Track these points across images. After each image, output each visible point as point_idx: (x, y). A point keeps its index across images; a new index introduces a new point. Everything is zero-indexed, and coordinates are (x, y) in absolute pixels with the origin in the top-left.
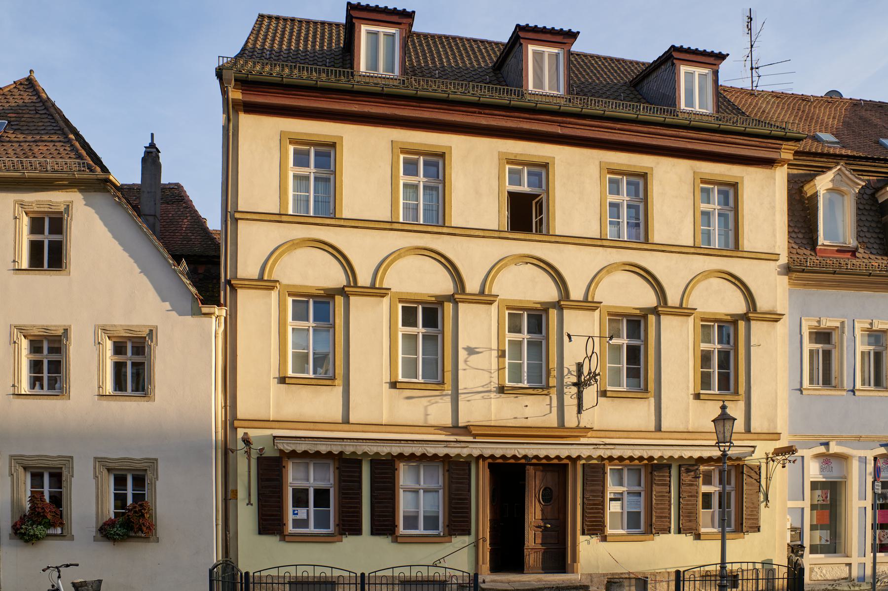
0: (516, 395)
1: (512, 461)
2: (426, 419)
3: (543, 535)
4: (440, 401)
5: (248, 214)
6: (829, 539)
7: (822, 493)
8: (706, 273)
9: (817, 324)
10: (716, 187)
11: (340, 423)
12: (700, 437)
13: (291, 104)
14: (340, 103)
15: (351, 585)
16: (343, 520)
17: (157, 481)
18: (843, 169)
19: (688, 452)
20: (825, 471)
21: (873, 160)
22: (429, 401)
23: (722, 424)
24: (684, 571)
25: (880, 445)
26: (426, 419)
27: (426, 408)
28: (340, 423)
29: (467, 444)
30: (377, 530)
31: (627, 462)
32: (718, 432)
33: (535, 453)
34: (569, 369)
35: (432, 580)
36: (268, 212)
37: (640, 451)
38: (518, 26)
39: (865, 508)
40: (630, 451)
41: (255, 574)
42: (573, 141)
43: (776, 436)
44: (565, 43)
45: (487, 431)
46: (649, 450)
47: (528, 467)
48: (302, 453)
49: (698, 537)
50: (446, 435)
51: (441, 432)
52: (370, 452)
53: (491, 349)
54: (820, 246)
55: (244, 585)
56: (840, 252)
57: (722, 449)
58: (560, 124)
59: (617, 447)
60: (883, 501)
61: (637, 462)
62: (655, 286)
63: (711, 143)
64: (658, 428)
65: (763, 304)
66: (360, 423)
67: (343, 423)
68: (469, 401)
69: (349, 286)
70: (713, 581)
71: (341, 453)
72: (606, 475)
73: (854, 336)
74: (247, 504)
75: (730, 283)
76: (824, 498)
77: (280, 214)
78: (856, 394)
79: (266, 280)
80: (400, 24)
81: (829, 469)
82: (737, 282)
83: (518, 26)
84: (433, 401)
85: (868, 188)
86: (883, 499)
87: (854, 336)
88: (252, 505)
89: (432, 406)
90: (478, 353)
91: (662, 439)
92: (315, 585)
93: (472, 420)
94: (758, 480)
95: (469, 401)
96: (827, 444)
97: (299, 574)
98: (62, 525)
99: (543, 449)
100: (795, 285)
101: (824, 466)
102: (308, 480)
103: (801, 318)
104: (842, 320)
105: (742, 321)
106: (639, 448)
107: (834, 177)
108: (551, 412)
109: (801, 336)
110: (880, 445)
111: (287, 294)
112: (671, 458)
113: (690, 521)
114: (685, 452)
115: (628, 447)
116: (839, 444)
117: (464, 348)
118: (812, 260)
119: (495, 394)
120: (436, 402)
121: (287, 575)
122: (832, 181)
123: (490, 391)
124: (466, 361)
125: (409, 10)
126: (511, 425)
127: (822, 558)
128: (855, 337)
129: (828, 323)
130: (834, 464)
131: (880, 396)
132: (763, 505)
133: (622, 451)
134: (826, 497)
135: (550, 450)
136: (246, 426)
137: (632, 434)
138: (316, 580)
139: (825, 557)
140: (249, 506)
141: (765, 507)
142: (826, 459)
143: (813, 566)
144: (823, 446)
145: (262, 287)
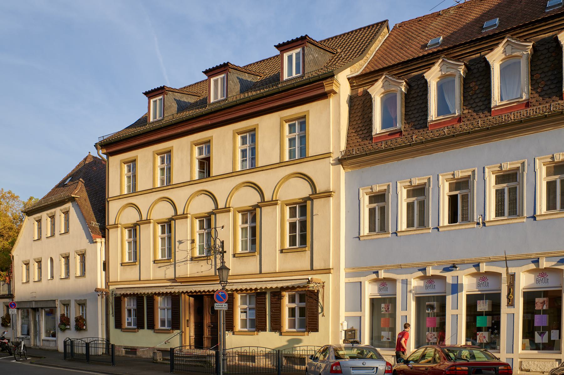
0: (198, 261)
1: (199, 294)
2: (165, 278)
3: (211, 330)
4: (170, 267)
6: (390, 338)
7: (385, 306)
8: (194, 194)
9: (370, 191)
10: (297, 121)
11: (258, 274)
12: (281, 275)
13: (288, 101)
18: (387, 76)
19: (270, 284)
20: (481, 286)
21: (525, 25)
22: (166, 268)
23: (227, 272)
25: (418, 270)
26: (165, 278)
27: (165, 271)
28: (258, 274)
29: (174, 287)
31: (245, 291)
32: (220, 275)
33: (199, 290)
34: (218, 245)
36: (216, 175)
37: (246, 285)
39: (406, 316)
40: (241, 286)
42: (218, 125)
43: (327, 271)
44: (226, 70)
45: (187, 279)
46: (250, 284)
47: (156, 297)
48: (270, 288)
49: (281, 334)
50: (171, 283)
51: (169, 282)
53: (187, 240)
54: (375, 135)
56: (391, 135)
57: (223, 285)
58: (209, 119)
59: (235, 284)
60: (431, 311)
61: (254, 291)
62: (259, 191)
63: (218, 117)
64: (261, 273)
65: (320, 188)
67: (311, 270)
68: (179, 266)
69: (313, 194)
72: (234, 299)
73: (484, 179)
75: (302, 179)
76: (386, 309)
77: (280, 163)
78: (486, 225)
79: (274, 200)
80: (163, 93)
81: (432, 287)
82: (305, 178)
84: (168, 268)
85: (414, 81)
86: (431, 309)
87: (484, 179)
89: (168, 269)
90: (183, 242)
91: (261, 278)
93: (180, 275)
94: (317, 299)
95: (179, 266)
96: (377, 273)
97: (243, 351)
98: (69, 325)
99: (203, 287)
100: (353, 168)
101: (428, 285)
102: (131, 305)
103: (359, 189)
104: (388, 184)
105: (309, 201)
106: (283, 282)
107: (383, 84)
108: (212, 268)
109: (359, 201)
110: (418, 270)
111: (491, 173)
113: (276, 324)
114: (268, 285)
115: (240, 284)
116: (387, 271)
117: (178, 241)
118: (368, 146)
119: (190, 261)
120: (169, 268)
121: (254, 351)
122: (383, 87)
123: (187, 260)
124: (178, 247)
125: (304, 35)
126: (196, 276)
127: (536, 354)
128: (485, 180)
130: (389, 285)
131: (416, 234)
132: (320, 316)
133: (237, 286)
134: (388, 309)
135: (205, 288)
136: (232, 278)
137: (246, 277)
139: (381, 350)
141: (322, 316)
142: (483, 277)
143: (523, 360)
144: (375, 274)
145: (324, 196)
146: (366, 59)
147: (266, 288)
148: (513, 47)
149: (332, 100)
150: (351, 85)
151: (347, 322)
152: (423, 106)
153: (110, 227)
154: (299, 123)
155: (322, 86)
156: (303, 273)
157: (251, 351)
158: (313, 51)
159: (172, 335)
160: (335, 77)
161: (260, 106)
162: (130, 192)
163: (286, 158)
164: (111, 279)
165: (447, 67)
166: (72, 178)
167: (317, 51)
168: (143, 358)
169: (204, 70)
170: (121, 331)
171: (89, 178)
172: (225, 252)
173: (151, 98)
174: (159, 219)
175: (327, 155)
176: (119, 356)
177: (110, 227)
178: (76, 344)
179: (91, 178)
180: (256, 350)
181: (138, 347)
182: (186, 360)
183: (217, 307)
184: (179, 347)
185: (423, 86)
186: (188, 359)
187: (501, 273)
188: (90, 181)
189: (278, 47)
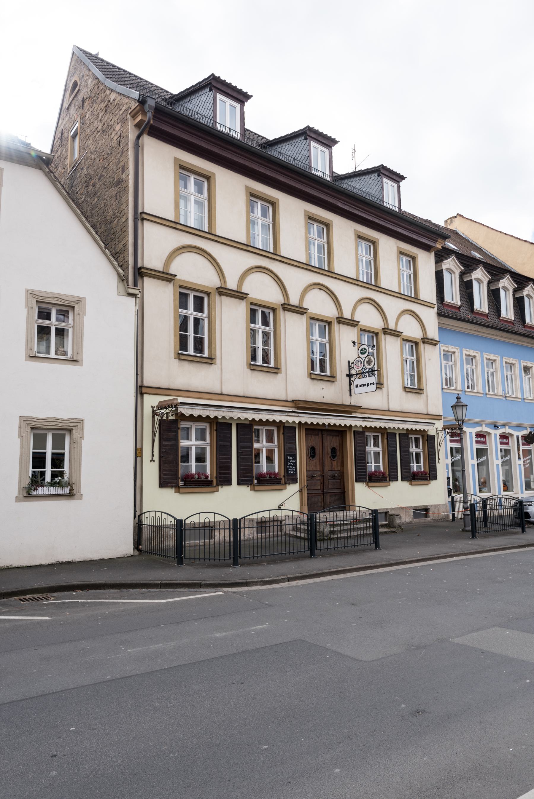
5: (294, 262)
14: (174, 129)
15: (288, 524)
16: (220, 473)
17: (83, 440)
24: (240, 519)
30: (242, 480)
35: (272, 520)
38: (213, 75)
41: (191, 522)
52: (195, 415)
55: (238, 527)
59: (374, 420)
66: (174, 391)
70: (255, 528)
71: (216, 417)
74: (151, 461)
83: (213, 75)
88: (154, 461)
92: (191, 530)
97: (202, 521)
112: (231, 418)
129: (529, 364)
138: (201, 526)
140: (152, 462)
156: (264, 401)
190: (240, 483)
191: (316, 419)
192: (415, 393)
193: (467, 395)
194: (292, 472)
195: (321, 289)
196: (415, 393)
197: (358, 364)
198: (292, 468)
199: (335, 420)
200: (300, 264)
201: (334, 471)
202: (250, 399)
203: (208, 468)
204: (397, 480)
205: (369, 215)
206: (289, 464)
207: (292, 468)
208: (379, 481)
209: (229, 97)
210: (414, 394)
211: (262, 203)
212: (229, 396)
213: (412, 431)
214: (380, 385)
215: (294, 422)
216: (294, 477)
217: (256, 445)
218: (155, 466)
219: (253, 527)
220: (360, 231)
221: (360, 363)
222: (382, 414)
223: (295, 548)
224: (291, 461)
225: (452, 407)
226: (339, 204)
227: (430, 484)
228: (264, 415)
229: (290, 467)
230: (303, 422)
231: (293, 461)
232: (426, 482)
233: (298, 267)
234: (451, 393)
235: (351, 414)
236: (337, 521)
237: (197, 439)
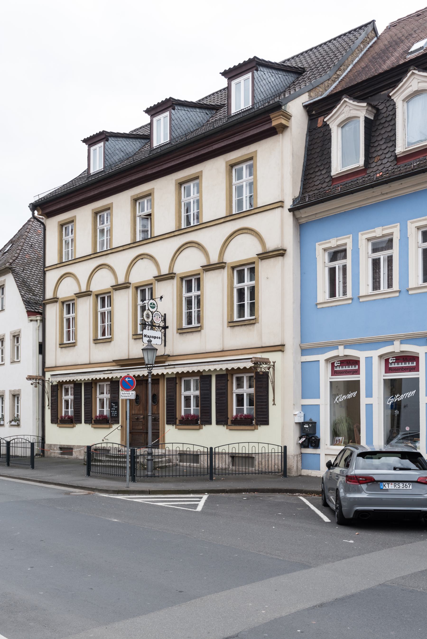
59: (176, 366)
97: (185, 449)
140: (274, 405)
146: (337, 77)
147: (210, 370)
148: (351, 108)
149: (287, 134)
150: (309, 114)
151: (304, 412)
152: (391, 134)
153: (47, 301)
154: (248, 167)
155: (270, 120)
156: (240, 352)
157: (174, 449)
158: (267, 74)
159: (111, 430)
160: (283, 107)
161: (259, 127)
162: (68, 258)
163: (183, 226)
164: (48, 364)
165: (419, 81)
166: (13, 244)
167: (273, 74)
168: (80, 459)
169: (222, 71)
170: (176, 428)
171: (31, 243)
172: (167, 327)
173: (232, 79)
174: (101, 290)
175: (280, 204)
176: (55, 457)
177: (47, 301)
178: (26, 443)
179: (33, 244)
180: (112, 446)
181: (74, 446)
182: (119, 461)
183: (123, 395)
184: (119, 444)
185: (392, 108)
186: (114, 459)
187: (418, 352)
188: (31, 247)
189: (148, 111)
190: (218, 423)
191: (124, 373)
192: (245, 325)
193: (412, 294)
194: (114, 415)
195: (142, 259)
196: (245, 325)
197: (157, 318)
198: (114, 412)
199: (140, 372)
200: (124, 247)
201: (154, 414)
202: (191, 355)
203: (106, 411)
204: (81, 423)
205: (161, 165)
206: (112, 409)
207: (114, 412)
208: (188, 424)
209: (97, 143)
210: (244, 328)
211: (406, 101)
212: (252, 349)
213: (233, 371)
214: (181, 330)
215: (173, 373)
216: (116, 419)
217: (252, 390)
218: (50, 410)
219: (12, 447)
220: (181, 177)
221: (158, 317)
222: (195, 357)
223: (95, 470)
224: (114, 407)
225: (142, 349)
226: (149, 172)
227: (257, 429)
228: (91, 376)
229: (113, 411)
230: (230, 369)
231: (115, 407)
232: (72, 426)
233: (124, 250)
234: (332, 306)
235: (165, 363)
236: (115, 454)
237: (194, 391)
